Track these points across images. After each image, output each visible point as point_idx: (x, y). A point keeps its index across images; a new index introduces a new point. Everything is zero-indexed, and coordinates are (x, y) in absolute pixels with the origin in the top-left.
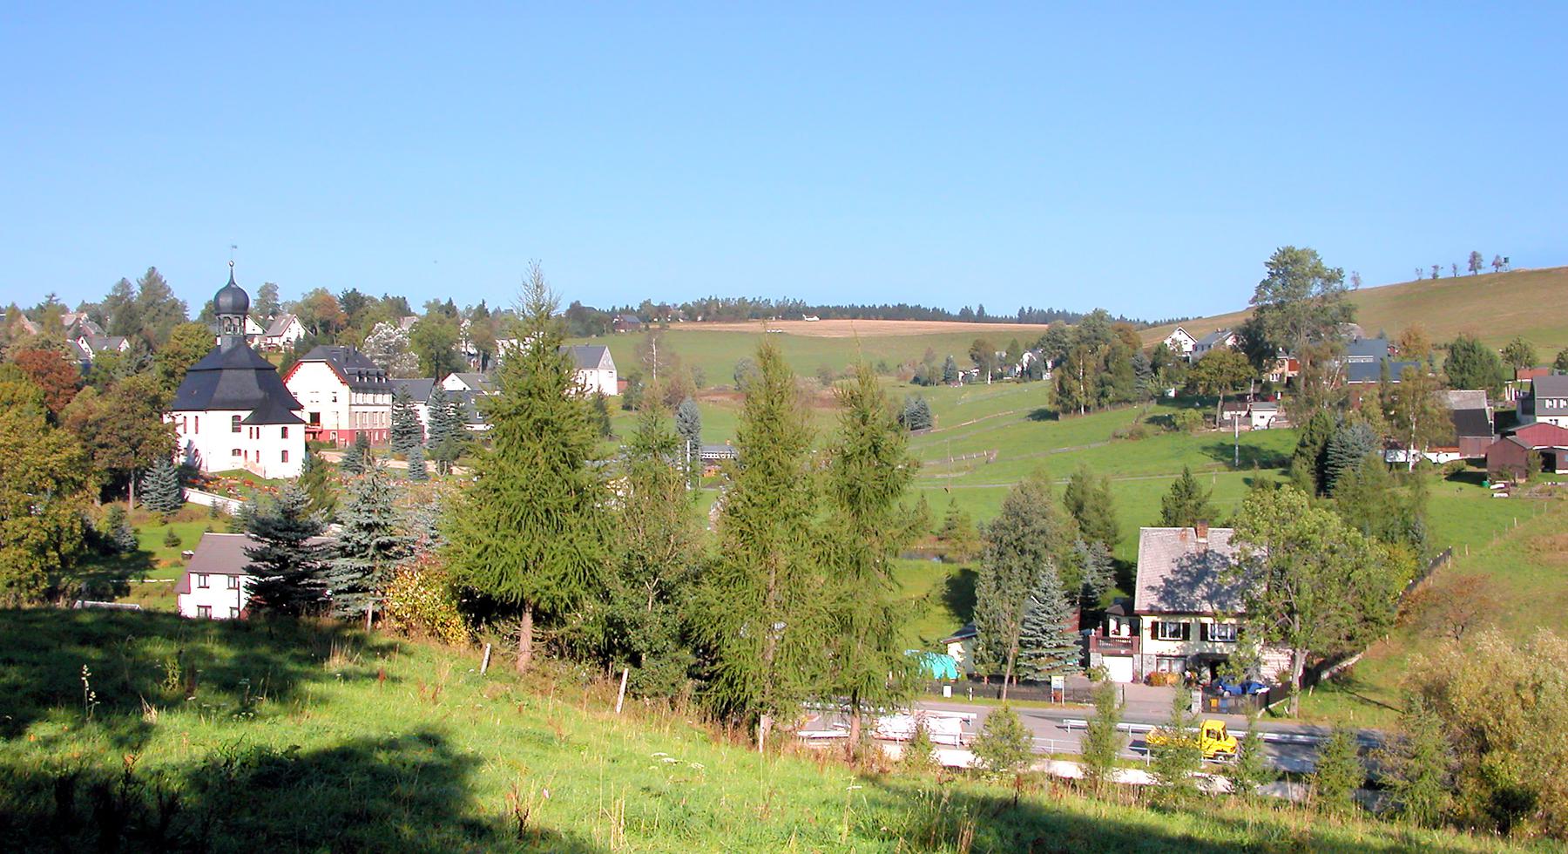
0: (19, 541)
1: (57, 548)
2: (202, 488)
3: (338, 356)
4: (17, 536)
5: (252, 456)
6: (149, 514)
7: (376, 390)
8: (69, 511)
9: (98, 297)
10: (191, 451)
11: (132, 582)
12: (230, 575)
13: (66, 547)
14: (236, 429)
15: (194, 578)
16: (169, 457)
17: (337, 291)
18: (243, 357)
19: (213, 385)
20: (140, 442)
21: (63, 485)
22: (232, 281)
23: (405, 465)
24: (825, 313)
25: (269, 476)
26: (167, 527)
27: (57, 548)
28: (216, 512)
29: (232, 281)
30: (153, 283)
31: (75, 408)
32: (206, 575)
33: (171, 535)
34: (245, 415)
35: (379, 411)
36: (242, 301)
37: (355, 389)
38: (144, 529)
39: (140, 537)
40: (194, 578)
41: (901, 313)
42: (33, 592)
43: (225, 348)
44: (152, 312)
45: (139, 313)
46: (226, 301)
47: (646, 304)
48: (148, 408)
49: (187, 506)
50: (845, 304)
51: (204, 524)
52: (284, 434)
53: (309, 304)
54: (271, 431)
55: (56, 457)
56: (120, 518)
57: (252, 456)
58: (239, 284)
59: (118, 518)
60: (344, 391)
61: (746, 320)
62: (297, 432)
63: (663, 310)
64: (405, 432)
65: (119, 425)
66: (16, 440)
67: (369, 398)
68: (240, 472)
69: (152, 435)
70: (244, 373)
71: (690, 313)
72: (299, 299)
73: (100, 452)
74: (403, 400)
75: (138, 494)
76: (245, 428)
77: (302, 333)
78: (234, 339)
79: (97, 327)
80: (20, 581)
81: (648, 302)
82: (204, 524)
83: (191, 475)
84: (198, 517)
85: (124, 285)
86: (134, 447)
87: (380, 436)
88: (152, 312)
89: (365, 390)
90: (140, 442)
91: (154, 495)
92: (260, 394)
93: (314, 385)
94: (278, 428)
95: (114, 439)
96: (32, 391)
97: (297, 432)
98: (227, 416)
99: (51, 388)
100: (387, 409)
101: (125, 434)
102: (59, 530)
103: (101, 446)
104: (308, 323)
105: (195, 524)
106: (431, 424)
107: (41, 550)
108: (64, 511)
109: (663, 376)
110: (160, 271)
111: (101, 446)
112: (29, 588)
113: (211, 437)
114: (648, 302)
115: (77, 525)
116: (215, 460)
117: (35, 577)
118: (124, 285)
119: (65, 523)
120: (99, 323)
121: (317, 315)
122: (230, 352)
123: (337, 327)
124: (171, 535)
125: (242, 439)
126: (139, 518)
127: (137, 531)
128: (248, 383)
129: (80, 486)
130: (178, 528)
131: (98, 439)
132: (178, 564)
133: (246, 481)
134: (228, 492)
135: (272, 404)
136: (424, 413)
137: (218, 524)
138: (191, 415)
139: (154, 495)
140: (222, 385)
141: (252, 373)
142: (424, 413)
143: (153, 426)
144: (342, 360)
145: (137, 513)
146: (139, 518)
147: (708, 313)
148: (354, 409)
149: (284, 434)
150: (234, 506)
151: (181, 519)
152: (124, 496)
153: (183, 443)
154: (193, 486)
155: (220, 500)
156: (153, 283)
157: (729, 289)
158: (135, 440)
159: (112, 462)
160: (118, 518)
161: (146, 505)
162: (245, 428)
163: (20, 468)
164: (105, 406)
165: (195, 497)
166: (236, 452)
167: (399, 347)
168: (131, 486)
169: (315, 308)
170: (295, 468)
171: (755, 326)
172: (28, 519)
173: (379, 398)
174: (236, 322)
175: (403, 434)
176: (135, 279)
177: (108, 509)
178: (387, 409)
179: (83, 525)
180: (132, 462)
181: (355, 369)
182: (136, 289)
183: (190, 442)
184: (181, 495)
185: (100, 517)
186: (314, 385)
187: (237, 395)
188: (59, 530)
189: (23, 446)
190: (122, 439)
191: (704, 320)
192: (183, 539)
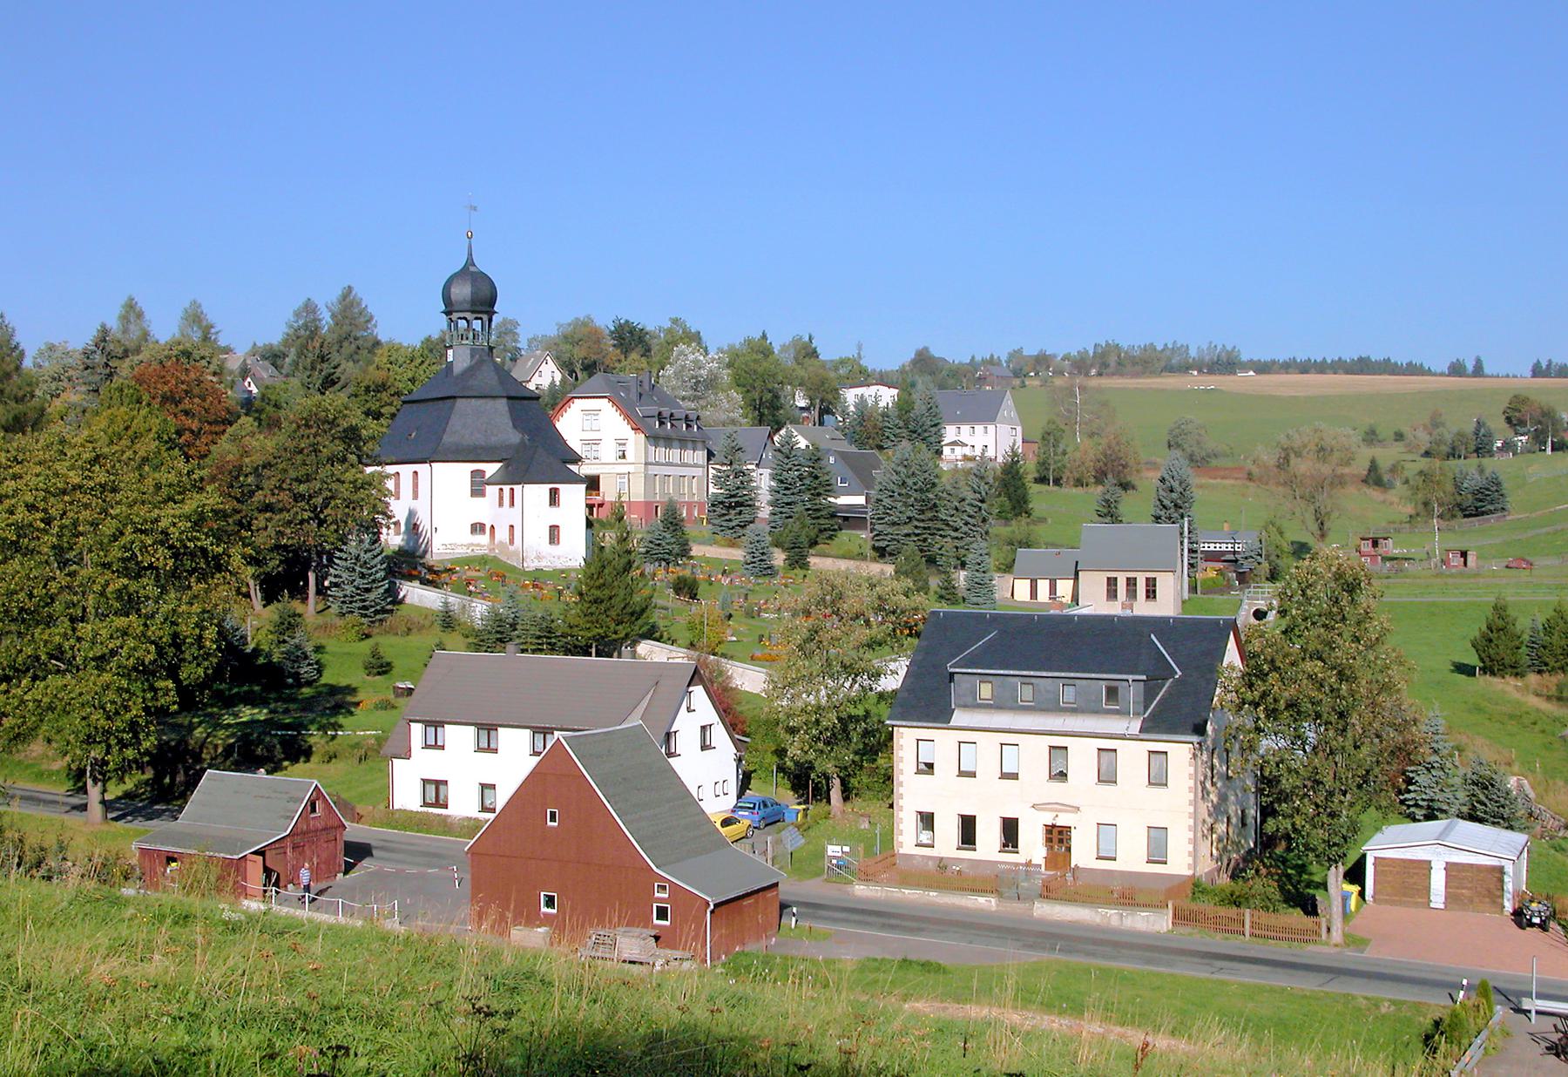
0: (101, 661)
1: (173, 672)
3: (627, 390)
4: (98, 651)
5: (502, 535)
6: (340, 622)
7: (683, 443)
8: (196, 608)
9: (274, 335)
11: (315, 737)
12: (536, 730)
13: (191, 672)
14: (477, 490)
15: (417, 729)
17: (605, 321)
18: (487, 379)
21: (194, 564)
22: (470, 262)
23: (738, 554)
24: (1262, 368)
25: (531, 565)
26: (370, 642)
27: (173, 672)
28: (448, 621)
29: (470, 262)
31: (224, 448)
32: (438, 724)
33: (375, 654)
34: (491, 469)
35: (692, 478)
36: (486, 292)
37: (654, 439)
38: (331, 645)
40: (417, 729)
41: (1363, 366)
42: (130, 753)
43: (457, 369)
44: (348, 348)
45: (328, 349)
46: (462, 292)
47: (1016, 355)
48: (339, 447)
49: (402, 611)
50: (1282, 356)
52: (554, 498)
54: (536, 493)
55: (170, 510)
56: (291, 627)
57: (502, 535)
58: (482, 265)
59: (288, 625)
60: (636, 443)
61: (1153, 373)
62: (573, 496)
63: (1042, 361)
64: (732, 507)
65: (293, 474)
66: (102, 478)
67: (674, 455)
68: (483, 560)
70: (490, 403)
71: (1080, 365)
72: (552, 332)
73: (260, 521)
74: (730, 457)
75: (321, 591)
76: (492, 491)
77: (558, 377)
78: (473, 353)
80: (107, 733)
81: (1020, 351)
83: (409, 562)
84: (421, 628)
85: (309, 308)
87: (690, 513)
88: (348, 348)
89: (668, 441)
92: (514, 437)
93: (594, 427)
94: (543, 490)
95: (285, 497)
96: (155, 423)
97: (573, 496)
98: (464, 470)
99: (189, 422)
100: (699, 472)
101: (302, 488)
102: (177, 641)
103: (268, 508)
104: (567, 366)
105: (414, 640)
106: (773, 491)
107: (145, 672)
108: (181, 609)
109: (1091, 435)
110: (360, 292)
111: (268, 508)
112: (123, 745)
114: (1020, 351)
115: (211, 633)
116: (449, 537)
117: (133, 726)
118: (309, 308)
119: (187, 629)
122: (470, 372)
123: (610, 357)
124: (375, 654)
125: (486, 508)
126: (325, 628)
127: (319, 649)
128: (495, 421)
129: (218, 564)
130: (389, 645)
131: (259, 496)
132: (386, 706)
133: (493, 572)
134: (464, 588)
135: (537, 456)
136: (763, 481)
138: (406, 471)
139: (349, 589)
140: (456, 423)
141: (502, 405)
142: (763, 481)
144: (634, 396)
145: (320, 620)
147: (1105, 365)
148: (653, 470)
149: (554, 498)
150: (479, 609)
151: (393, 631)
152: (300, 593)
155: (455, 600)
156: (350, 311)
157: (1131, 338)
159: (280, 534)
160: (288, 625)
161: (335, 608)
162: (492, 491)
163: (108, 527)
164: (270, 444)
165: (415, 594)
166: (477, 528)
167: (712, 383)
168: (312, 576)
170: (573, 551)
171: (1171, 382)
172: (121, 622)
173: (689, 456)
174: (477, 325)
175: (730, 507)
176: (326, 302)
178: (699, 472)
179: (222, 634)
180: (311, 535)
181: (654, 410)
182: (326, 320)
184: (392, 592)
185: (256, 622)
186: (594, 427)
187: (478, 439)
188: (177, 641)
189: (114, 490)
190: (297, 497)
191: (1100, 374)
192: (396, 663)
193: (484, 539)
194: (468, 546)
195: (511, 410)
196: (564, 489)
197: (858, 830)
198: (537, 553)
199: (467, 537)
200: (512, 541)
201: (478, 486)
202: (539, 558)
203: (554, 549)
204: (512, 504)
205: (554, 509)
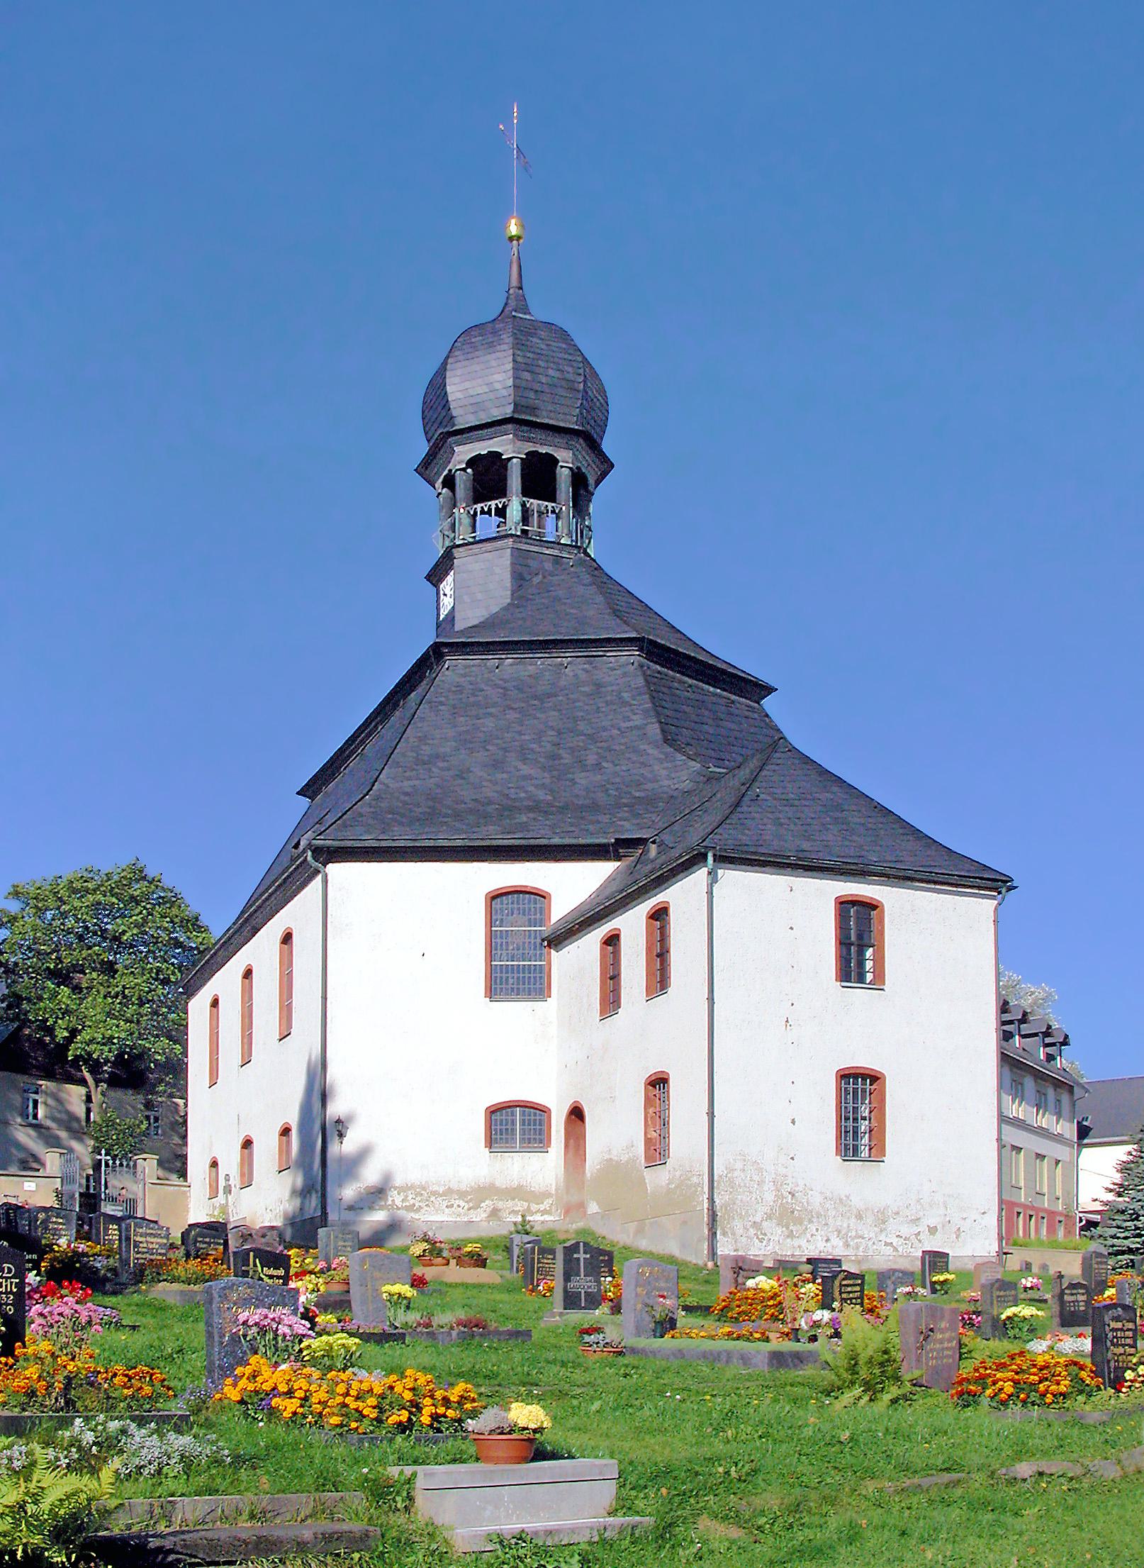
14: (514, 972)
25: (757, 1238)
34: (570, 884)
52: (857, 945)
57: (616, 1131)
116: (424, 1150)
125: (533, 1048)
149: (857, 945)
166: (512, 1124)
193: (542, 1168)
194: (478, 1194)
195: (654, 689)
196: (906, 911)
197: (362, 1474)
198: (785, 1192)
199: (473, 1162)
200: (657, 1150)
201: (517, 958)
202: (789, 1215)
203: (857, 1183)
204: (659, 980)
205: (858, 996)
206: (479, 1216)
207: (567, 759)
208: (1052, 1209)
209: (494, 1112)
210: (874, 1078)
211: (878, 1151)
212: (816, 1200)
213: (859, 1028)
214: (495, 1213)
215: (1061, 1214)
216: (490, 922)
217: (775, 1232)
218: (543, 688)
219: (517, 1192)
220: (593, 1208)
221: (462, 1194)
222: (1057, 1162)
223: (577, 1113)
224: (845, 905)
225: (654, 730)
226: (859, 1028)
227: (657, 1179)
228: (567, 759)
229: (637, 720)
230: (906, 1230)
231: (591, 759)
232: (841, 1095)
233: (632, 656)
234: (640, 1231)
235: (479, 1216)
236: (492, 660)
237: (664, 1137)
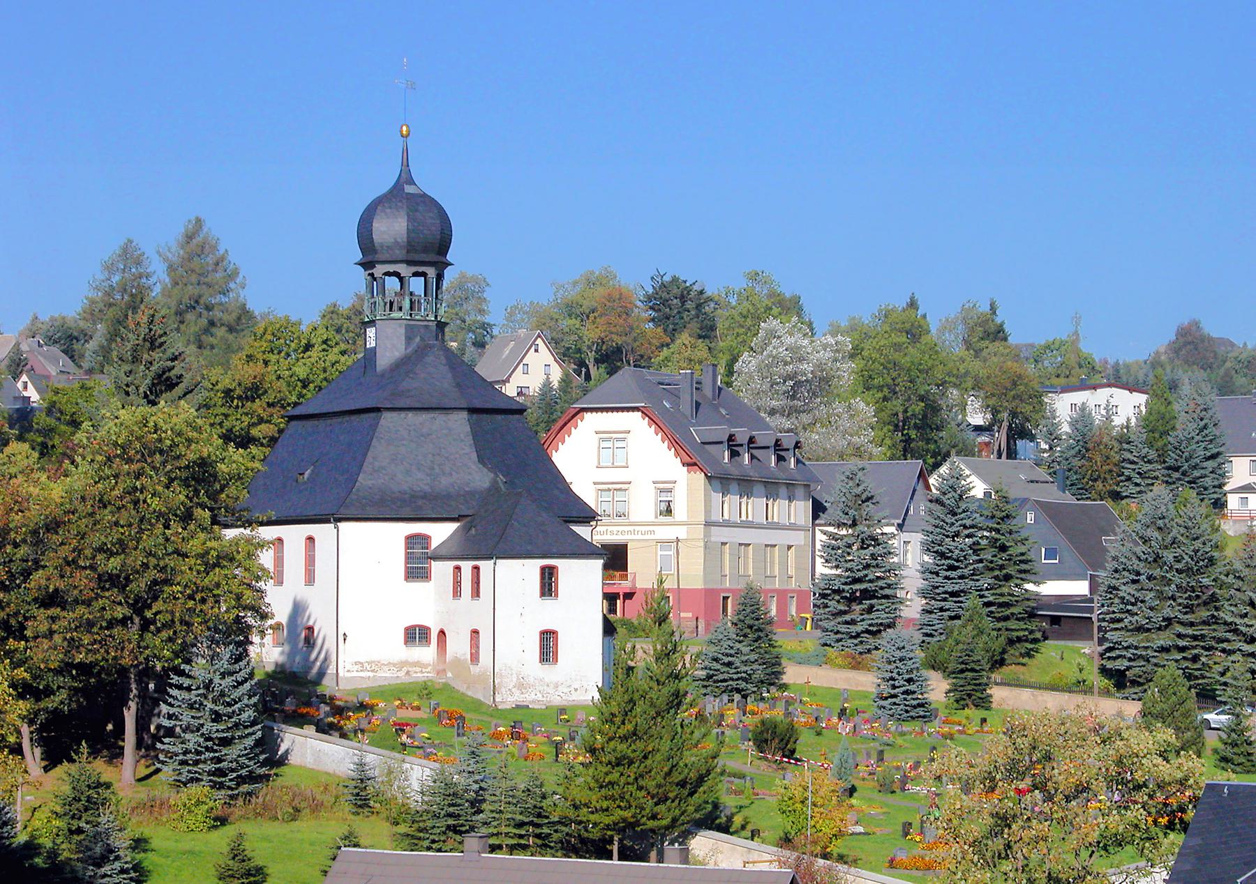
2: (324, 729)
3: (675, 396)
5: (458, 646)
7: (771, 488)
10: (302, 635)
14: (416, 571)
16: (236, 635)
19: (359, 452)
20: (154, 590)
23: (867, 682)
25: (508, 698)
26: (229, 831)
28: (362, 795)
29: (406, 177)
30: (200, 261)
33: (237, 853)
34: (440, 533)
35: (787, 549)
36: (431, 231)
37: (721, 481)
38: (160, 837)
39: (149, 860)
43: (384, 360)
44: (194, 322)
46: (392, 229)
48: (179, 496)
49: (287, 777)
51: (331, 828)
53: (571, 309)
54: (515, 576)
56: (92, 805)
57: (458, 646)
58: (427, 182)
59: (88, 800)
60: (688, 487)
62: (582, 579)
64: (856, 600)
65: (96, 539)
67: (754, 507)
69: (187, 571)
70: (440, 419)
73: (40, 620)
75: (147, 745)
77: (556, 374)
79: (64, 360)
82: (331, 828)
83: (297, 694)
85: (130, 255)
86: (139, 606)
88: (194, 322)
89: (745, 485)
90: (154, 590)
91: (193, 740)
92: (480, 478)
93: (617, 460)
94: (530, 569)
95: (83, 580)
97: (582, 579)
98: (394, 534)
101: (114, 564)
103: (51, 600)
104: (568, 354)
105: (306, 828)
111: (51, 600)
113: (357, 593)
118: (130, 255)
120: (69, 353)
121: (591, 333)
122: (403, 366)
123: (644, 343)
124: (237, 853)
125: (427, 601)
127: (139, 844)
128: (443, 447)
133: (437, 711)
134: (398, 737)
135: (520, 511)
136: (910, 555)
137: (375, 830)
138: (294, 535)
139: (193, 740)
140: (380, 453)
141: (460, 422)
142: (910, 555)
143: (194, 546)
144: (686, 407)
145: (142, 793)
146: (153, 807)
148: (719, 534)
150: (417, 776)
151: (267, 813)
152: (110, 748)
153: (279, 602)
154: (298, 719)
155: (375, 759)
156: (200, 261)
158: (139, 585)
159: (73, 644)
160: (88, 800)
162: (442, 570)
164: (57, 491)
165: (305, 749)
166: (416, 635)
167: (822, 384)
169: (584, 317)
170: (580, 675)
174: (417, 285)
175: (852, 599)
177: (60, 780)
180: (127, 646)
182: (158, 278)
183: (298, 609)
184: (267, 744)
187: (419, 481)
193: (426, 654)
194: (403, 664)
199: (397, 650)
200: (475, 657)
201: (418, 563)
202: (521, 686)
204: (476, 593)
205: (548, 603)
206: (401, 674)
207: (437, 470)
208: (785, 587)
209: (407, 629)
210: (554, 633)
211: (556, 660)
212: (532, 680)
213: (549, 614)
214: (408, 673)
215: (793, 591)
216: (407, 548)
217: (517, 692)
218: (425, 430)
219: (416, 664)
220: (449, 675)
221: (394, 665)
222: (789, 547)
223: (442, 632)
224: (543, 569)
225: (474, 456)
226: (549, 614)
227: (475, 670)
228: (437, 470)
229: (467, 450)
230: (566, 690)
231: (447, 469)
232: (542, 640)
233: (464, 414)
234: (468, 688)
235: (401, 674)
236: (403, 414)
237: (478, 653)
